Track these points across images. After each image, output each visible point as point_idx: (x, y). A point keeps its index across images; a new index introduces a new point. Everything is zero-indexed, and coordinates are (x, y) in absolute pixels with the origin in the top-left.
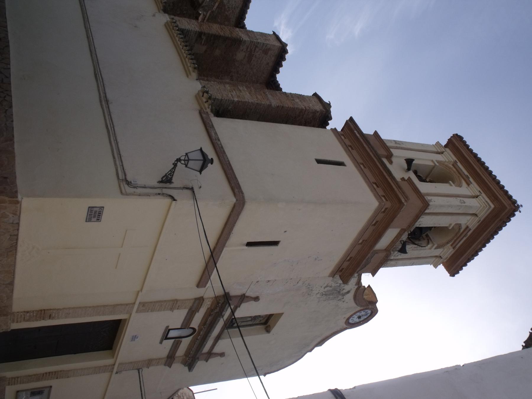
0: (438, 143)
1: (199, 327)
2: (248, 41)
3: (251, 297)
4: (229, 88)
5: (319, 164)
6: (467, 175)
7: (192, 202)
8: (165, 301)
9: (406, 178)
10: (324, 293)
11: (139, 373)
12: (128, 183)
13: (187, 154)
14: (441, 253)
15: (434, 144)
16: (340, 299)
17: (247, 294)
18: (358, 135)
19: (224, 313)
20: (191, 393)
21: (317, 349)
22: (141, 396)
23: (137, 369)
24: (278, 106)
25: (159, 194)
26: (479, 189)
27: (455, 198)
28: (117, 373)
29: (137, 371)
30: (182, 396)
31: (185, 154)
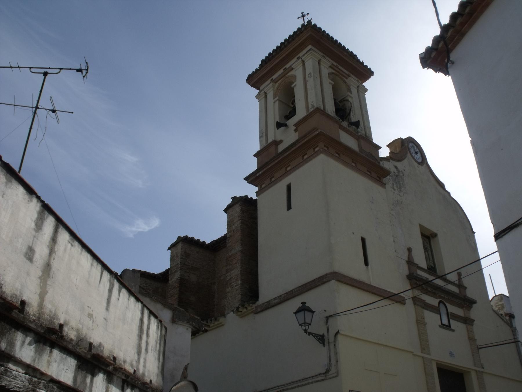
0: (257, 97)
1: (437, 299)
2: (180, 272)
3: (409, 255)
4: (229, 288)
5: (292, 207)
6: (284, 70)
7: (338, 317)
8: (418, 331)
9: (295, 128)
10: (399, 190)
11: (481, 348)
12: (328, 371)
13: (300, 325)
14: (354, 87)
15: (258, 100)
16: (403, 174)
17: (407, 259)
18: (260, 173)
19: (424, 278)
20: (495, 298)
21: (447, 188)
22: (501, 346)
23: (478, 350)
24: (241, 244)
25: (335, 345)
26: (295, 59)
27: (307, 83)
28: (483, 368)
29: (480, 350)
30: (499, 307)
31: (300, 326)
